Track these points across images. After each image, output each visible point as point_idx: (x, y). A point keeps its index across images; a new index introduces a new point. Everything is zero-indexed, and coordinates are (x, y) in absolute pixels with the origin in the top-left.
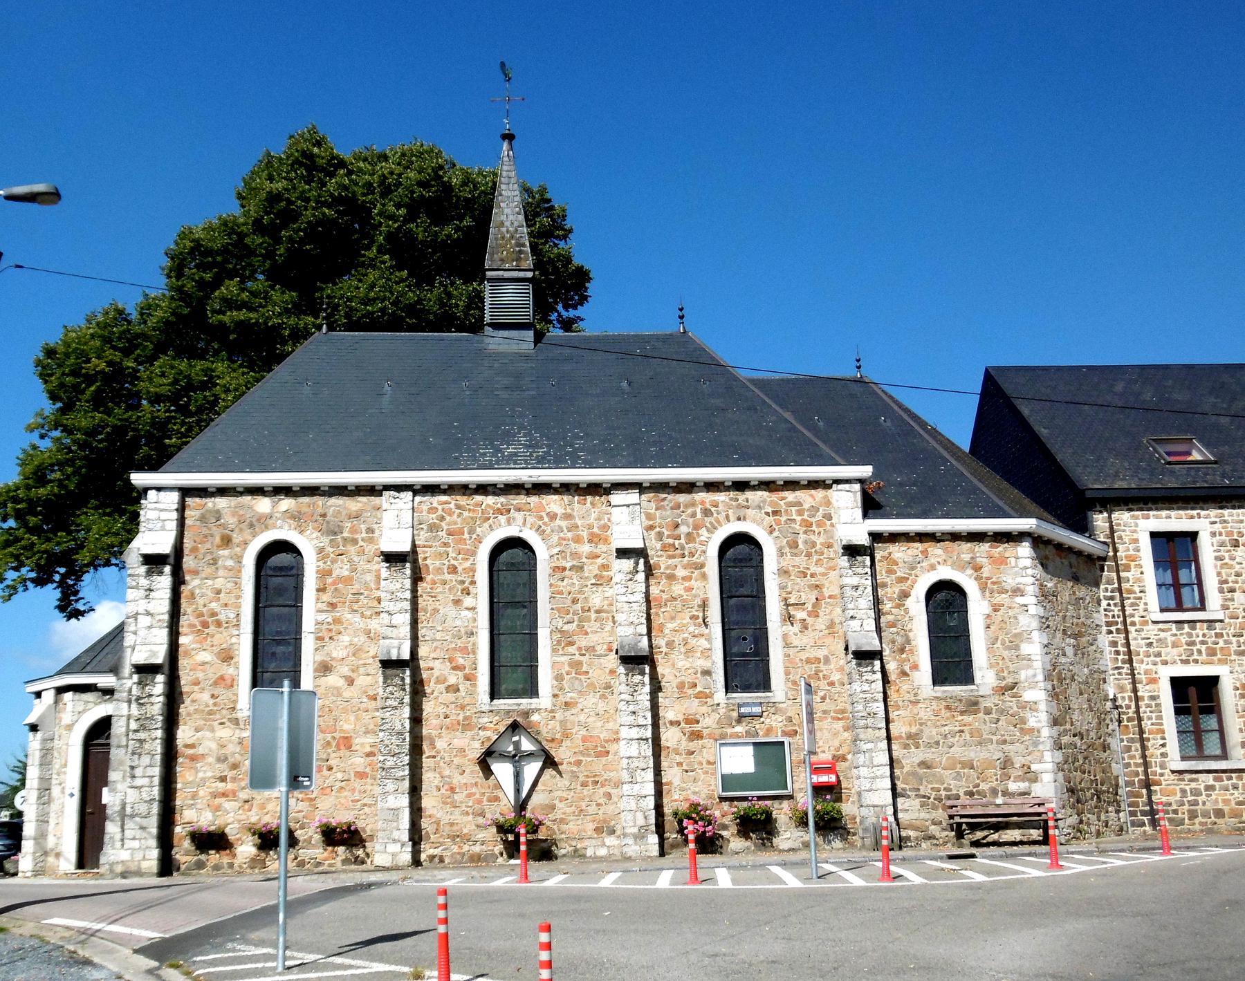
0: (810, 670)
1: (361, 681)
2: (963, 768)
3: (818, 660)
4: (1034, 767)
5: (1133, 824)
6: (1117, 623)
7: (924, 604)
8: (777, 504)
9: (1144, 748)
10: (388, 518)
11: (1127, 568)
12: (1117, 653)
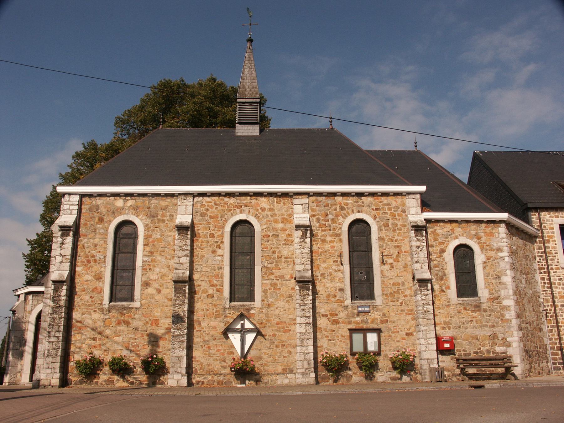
0: (395, 288)
1: (165, 291)
2: (473, 340)
3: (399, 284)
4: (508, 339)
5: (555, 368)
6: (544, 269)
7: (452, 256)
8: (378, 205)
9: (558, 330)
10: (181, 209)
11: (549, 242)
12: (545, 283)
